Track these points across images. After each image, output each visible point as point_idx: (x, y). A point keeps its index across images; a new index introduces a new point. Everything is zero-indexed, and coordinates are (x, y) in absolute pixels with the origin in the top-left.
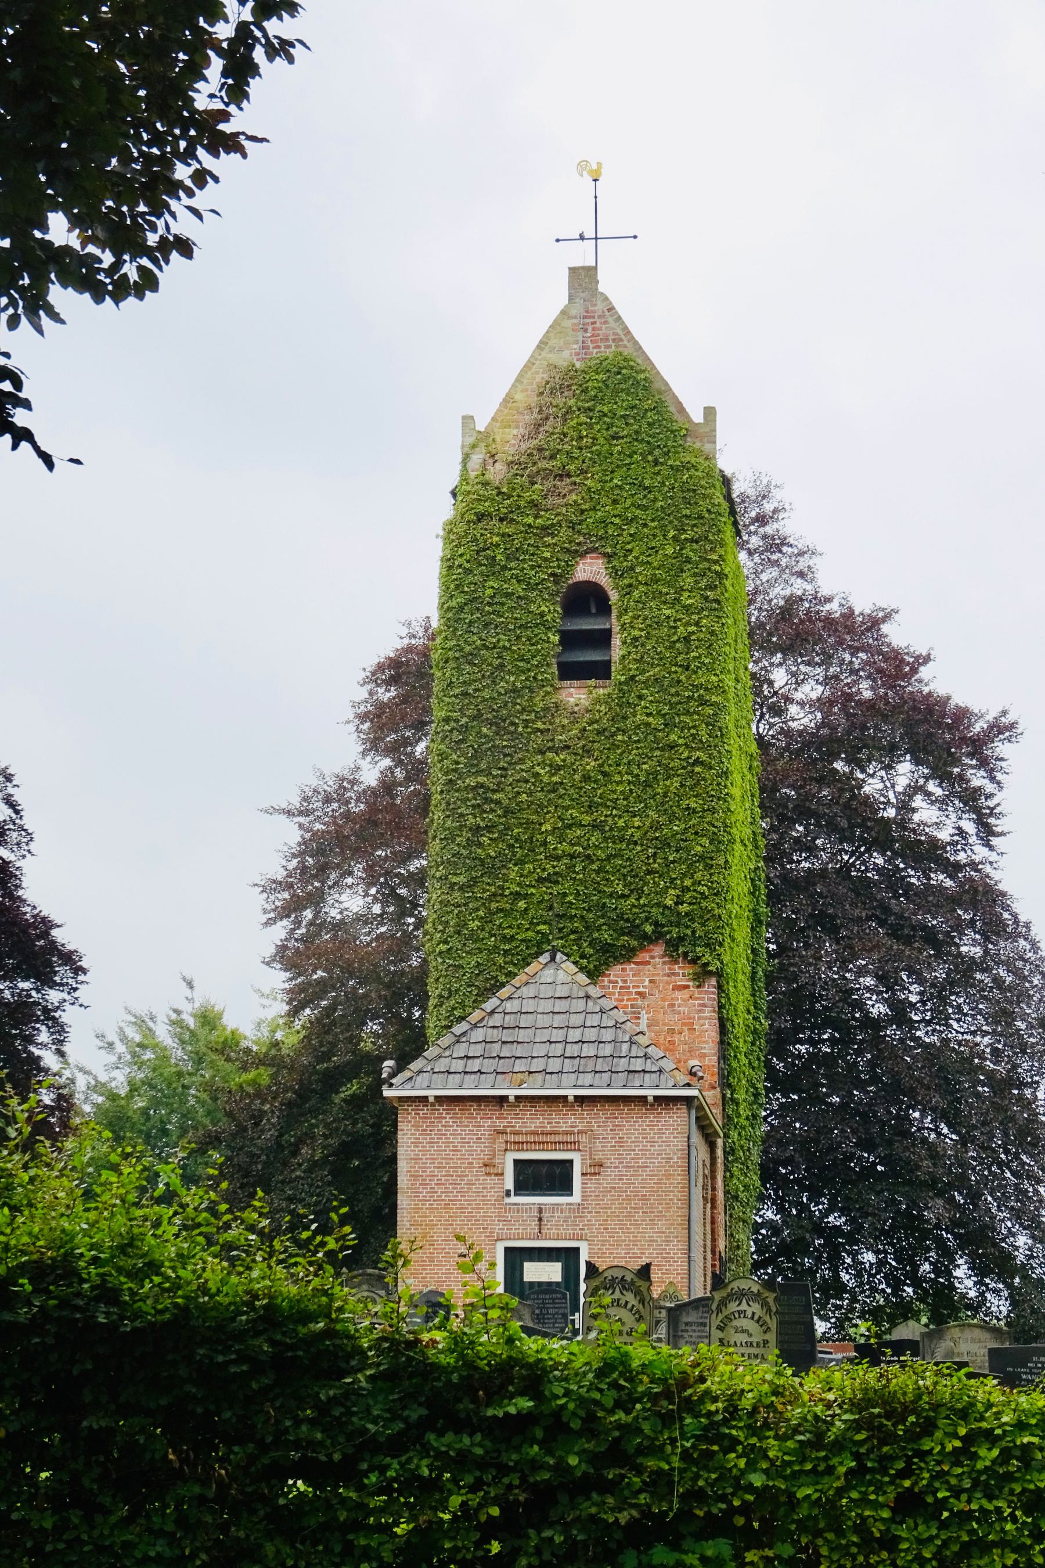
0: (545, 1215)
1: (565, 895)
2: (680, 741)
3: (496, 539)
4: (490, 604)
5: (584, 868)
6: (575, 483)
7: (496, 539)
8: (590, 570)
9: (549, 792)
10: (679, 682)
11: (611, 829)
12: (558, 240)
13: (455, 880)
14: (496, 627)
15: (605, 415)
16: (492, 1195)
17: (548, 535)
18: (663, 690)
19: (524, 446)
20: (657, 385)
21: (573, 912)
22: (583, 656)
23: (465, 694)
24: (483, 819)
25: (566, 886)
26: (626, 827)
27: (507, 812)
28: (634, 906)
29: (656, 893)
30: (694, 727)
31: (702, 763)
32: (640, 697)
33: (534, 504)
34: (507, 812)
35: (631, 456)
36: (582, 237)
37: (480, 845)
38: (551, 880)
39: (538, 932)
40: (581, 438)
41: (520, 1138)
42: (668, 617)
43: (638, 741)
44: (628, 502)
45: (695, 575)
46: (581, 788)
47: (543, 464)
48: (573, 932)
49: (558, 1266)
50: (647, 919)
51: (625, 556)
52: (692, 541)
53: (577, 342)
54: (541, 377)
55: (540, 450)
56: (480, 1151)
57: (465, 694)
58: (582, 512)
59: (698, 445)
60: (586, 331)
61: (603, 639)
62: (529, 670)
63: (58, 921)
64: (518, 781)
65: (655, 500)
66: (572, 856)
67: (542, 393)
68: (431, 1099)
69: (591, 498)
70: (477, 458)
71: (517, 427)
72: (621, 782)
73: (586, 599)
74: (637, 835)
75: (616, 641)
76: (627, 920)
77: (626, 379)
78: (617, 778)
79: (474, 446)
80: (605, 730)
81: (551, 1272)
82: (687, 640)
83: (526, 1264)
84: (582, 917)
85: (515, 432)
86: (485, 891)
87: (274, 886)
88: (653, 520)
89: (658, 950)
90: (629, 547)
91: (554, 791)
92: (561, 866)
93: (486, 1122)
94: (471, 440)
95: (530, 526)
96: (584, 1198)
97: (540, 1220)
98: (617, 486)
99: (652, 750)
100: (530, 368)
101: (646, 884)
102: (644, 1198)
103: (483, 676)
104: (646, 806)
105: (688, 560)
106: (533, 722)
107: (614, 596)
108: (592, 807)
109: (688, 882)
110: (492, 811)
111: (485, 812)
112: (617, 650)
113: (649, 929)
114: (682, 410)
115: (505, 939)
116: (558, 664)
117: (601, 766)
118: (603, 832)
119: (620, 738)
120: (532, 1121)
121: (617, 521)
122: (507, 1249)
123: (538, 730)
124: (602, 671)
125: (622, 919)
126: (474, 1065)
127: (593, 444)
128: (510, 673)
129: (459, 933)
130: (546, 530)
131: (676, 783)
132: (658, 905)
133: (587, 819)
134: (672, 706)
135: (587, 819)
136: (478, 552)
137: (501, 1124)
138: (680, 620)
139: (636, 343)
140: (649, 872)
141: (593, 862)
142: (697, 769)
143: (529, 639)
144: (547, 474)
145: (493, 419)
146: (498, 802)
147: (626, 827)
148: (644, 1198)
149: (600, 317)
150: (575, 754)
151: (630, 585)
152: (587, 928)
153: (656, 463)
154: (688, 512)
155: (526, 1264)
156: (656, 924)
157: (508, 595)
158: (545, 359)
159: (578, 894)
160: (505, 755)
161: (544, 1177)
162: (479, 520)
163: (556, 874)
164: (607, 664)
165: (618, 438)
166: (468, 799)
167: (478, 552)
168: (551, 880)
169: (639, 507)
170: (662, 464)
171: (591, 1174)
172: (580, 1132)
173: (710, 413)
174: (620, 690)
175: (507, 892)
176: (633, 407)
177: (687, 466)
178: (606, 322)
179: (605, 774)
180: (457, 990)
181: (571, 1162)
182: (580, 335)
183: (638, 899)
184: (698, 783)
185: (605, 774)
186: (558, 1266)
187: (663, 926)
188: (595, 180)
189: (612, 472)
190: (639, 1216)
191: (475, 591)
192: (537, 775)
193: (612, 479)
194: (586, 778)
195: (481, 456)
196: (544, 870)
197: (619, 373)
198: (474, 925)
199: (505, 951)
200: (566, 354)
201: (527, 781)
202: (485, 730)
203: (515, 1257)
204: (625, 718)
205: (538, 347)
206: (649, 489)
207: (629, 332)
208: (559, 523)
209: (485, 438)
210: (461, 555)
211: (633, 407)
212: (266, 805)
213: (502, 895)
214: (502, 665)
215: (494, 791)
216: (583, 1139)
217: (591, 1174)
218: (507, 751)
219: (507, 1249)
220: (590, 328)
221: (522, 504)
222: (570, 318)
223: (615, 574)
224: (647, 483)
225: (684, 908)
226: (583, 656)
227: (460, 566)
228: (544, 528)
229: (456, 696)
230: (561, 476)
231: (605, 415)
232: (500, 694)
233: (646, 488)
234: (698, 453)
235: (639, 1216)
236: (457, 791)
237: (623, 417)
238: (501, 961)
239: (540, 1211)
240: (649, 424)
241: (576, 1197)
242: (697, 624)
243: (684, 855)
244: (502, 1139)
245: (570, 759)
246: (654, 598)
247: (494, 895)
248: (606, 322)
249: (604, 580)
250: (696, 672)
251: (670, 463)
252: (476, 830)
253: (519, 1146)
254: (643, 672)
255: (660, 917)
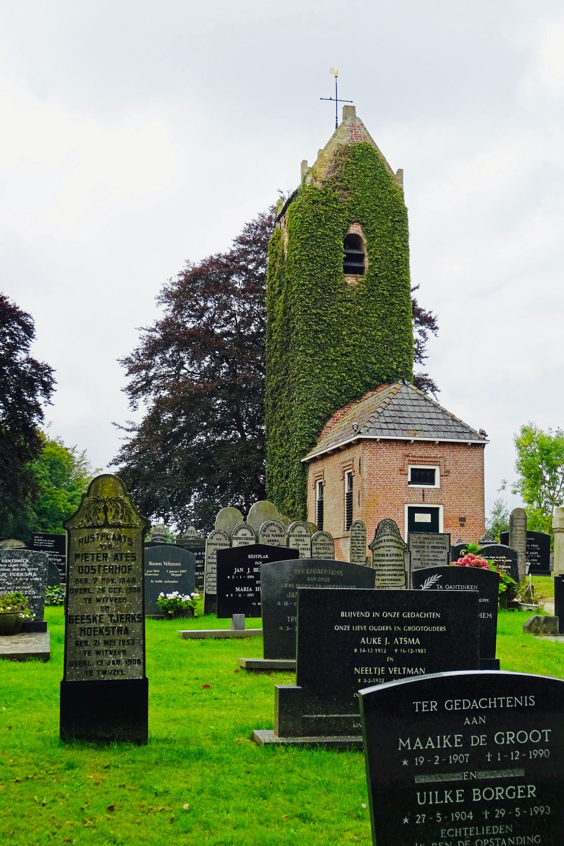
0: (426, 493)
1: (351, 361)
2: (396, 302)
3: (322, 212)
4: (319, 238)
5: (359, 351)
6: (350, 193)
7: (322, 212)
8: (355, 229)
9: (344, 318)
10: (394, 278)
11: (370, 336)
12: (321, 99)
13: (309, 352)
14: (322, 248)
15: (362, 167)
16: (403, 484)
17: (341, 213)
18: (388, 280)
19: (329, 176)
20: (380, 158)
21: (355, 369)
22: (353, 265)
23: (311, 275)
24: (319, 327)
25: (352, 358)
26: (375, 336)
27: (329, 325)
28: (378, 368)
29: (388, 363)
30: (402, 297)
31: (405, 312)
32: (380, 283)
33: (335, 199)
34: (329, 325)
35: (372, 185)
36: (331, 99)
37: (319, 338)
38: (346, 355)
39: (341, 376)
40: (353, 175)
42: (390, 251)
43: (379, 301)
44: (372, 203)
45: (400, 235)
46: (357, 318)
47: (338, 184)
48: (354, 377)
49: (417, 520)
50: (384, 373)
51: (371, 225)
52: (398, 221)
53: (349, 136)
54: (335, 148)
55: (337, 178)
56: (398, 464)
57: (311, 275)
58: (354, 205)
59: (397, 184)
60: (352, 132)
61: (360, 258)
62: (335, 267)
63: (53, 368)
64: (332, 313)
65: (383, 203)
66: (354, 346)
67: (336, 155)
68: (378, 440)
69: (358, 200)
70: (309, 178)
71: (325, 168)
72: (373, 317)
73: (353, 242)
75: (366, 259)
76: (376, 374)
77: (370, 153)
78: (371, 315)
79: (308, 173)
80: (365, 295)
81: (426, 518)
82: (397, 261)
83: (430, 515)
84: (358, 371)
85: (324, 169)
86: (320, 357)
87: (128, 361)
88: (382, 212)
90: (373, 221)
91: (346, 318)
92: (350, 349)
93: (400, 451)
94: (306, 171)
95: (334, 208)
96: (441, 485)
97: (423, 495)
98: (368, 196)
99: (385, 304)
100: (330, 144)
101: (383, 359)
102: (466, 487)
103: (317, 268)
104: (383, 328)
105: (397, 229)
106: (337, 289)
107: (365, 241)
108: (361, 326)
109: (401, 360)
110: (322, 324)
111: (320, 324)
112: (367, 263)
113: (385, 378)
114: (390, 169)
115: (329, 378)
116: (344, 266)
117: (365, 309)
118: (366, 336)
119: (372, 299)
120: (419, 452)
121: (368, 210)
122: (409, 508)
123: (339, 292)
124: (360, 271)
125: (374, 373)
126: (391, 426)
127: (358, 178)
128: (328, 268)
129: (310, 374)
130: (341, 211)
131: (395, 319)
132: (388, 368)
133: (360, 331)
134: (392, 287)
135: (360, 331)
136: (314, 216)
137: (407, 452)
138: (394, 253)
139: (372, 140)
140: (385, 354)
141: (362, 349)
142: (403, 314)
143: (335, 254)
144: (340, 188)
145: (315, 163)
146: (325, 321)
147: (375, 336)
148: (466, 487)
149: (358, 127)
150: (354, 304)
151: (373, 237)
152: (360, 376)
153: (383, 189)
154: (396, 210)
155: (430, 515)
156: (387, 376)
157: (327, 236)
158: (336, 141)
159: (357, 361)
160: (327, 302)
161: (423, 477)
162: (313, 204)
163: (348, 352)
164: (363, 268)
165: (368, 177)
166: (312, 318)
167: (314, 216)
168: (346, 355)
169: (376, 206)
170: (385, 189)
171: (445, 476)
172: (440, 457)
173: (400, 171)
174: (371, 279)
175: (330, 358)
176: (373, 165)
177: (395, 191)
178: (360, 130)
179: (366, 313)
180: (310, 398)
183: (380, 365)
184: (403, 320)
185: (366, 313)
186: (417, 520)
187: (390, 377)
188: (336, 77)
189: (366, 190)
190: (464, 495)
191: (313, 233)
192: (339, 311)
193: (366, 193)
194: (359, 314)
195: (311, 178)
196: (343, 350)
197: (367, 150)
198: (317, 371)
199: (329, 383)
200: (344, 140)
201: (336, 313)
202: (319, 290)
203: (413, 511)
205: (333, 136)
206: (380, 199)
207: (369, 135)
208: (345, 208)
209: (312, 170)
210: (307, 217)
211: (373, 165)
212: (139, 326)
213: (327, 360)
214: (324, 264)
215: (323, 316)
216: (442, 460)
217: (445, 476)
218: (328, 300)
219: (409, 508)
220: (354, 131)
221: (331, 199)
222: (346, 126)
223: (366, 232)
224: (380, 196)
225: (399, 370)
226: (353, 265)
227: (307, 221)
228: (340, 210)
229: (307, 275)
230: (344, 189)
231: (362, 167)
232: (324, 276)
233: (379, 198)
234: (397, 186)
235: (464, 495)
236: (308, 315)
237: (369, 168)
238: (327, 386)
239: (423, 491)
240: (380, 173)
241: (437, 485)
242: (401, 255)
243: (399, 348)
245: (353, 306)
246: (384, 243)
247: (324, 359)
248: (360, 130)
249: (361, 234)
250: (401, 275)
251: (388, 189)
252: (316, 332)
254: (380, 273)
255: (389, 373)
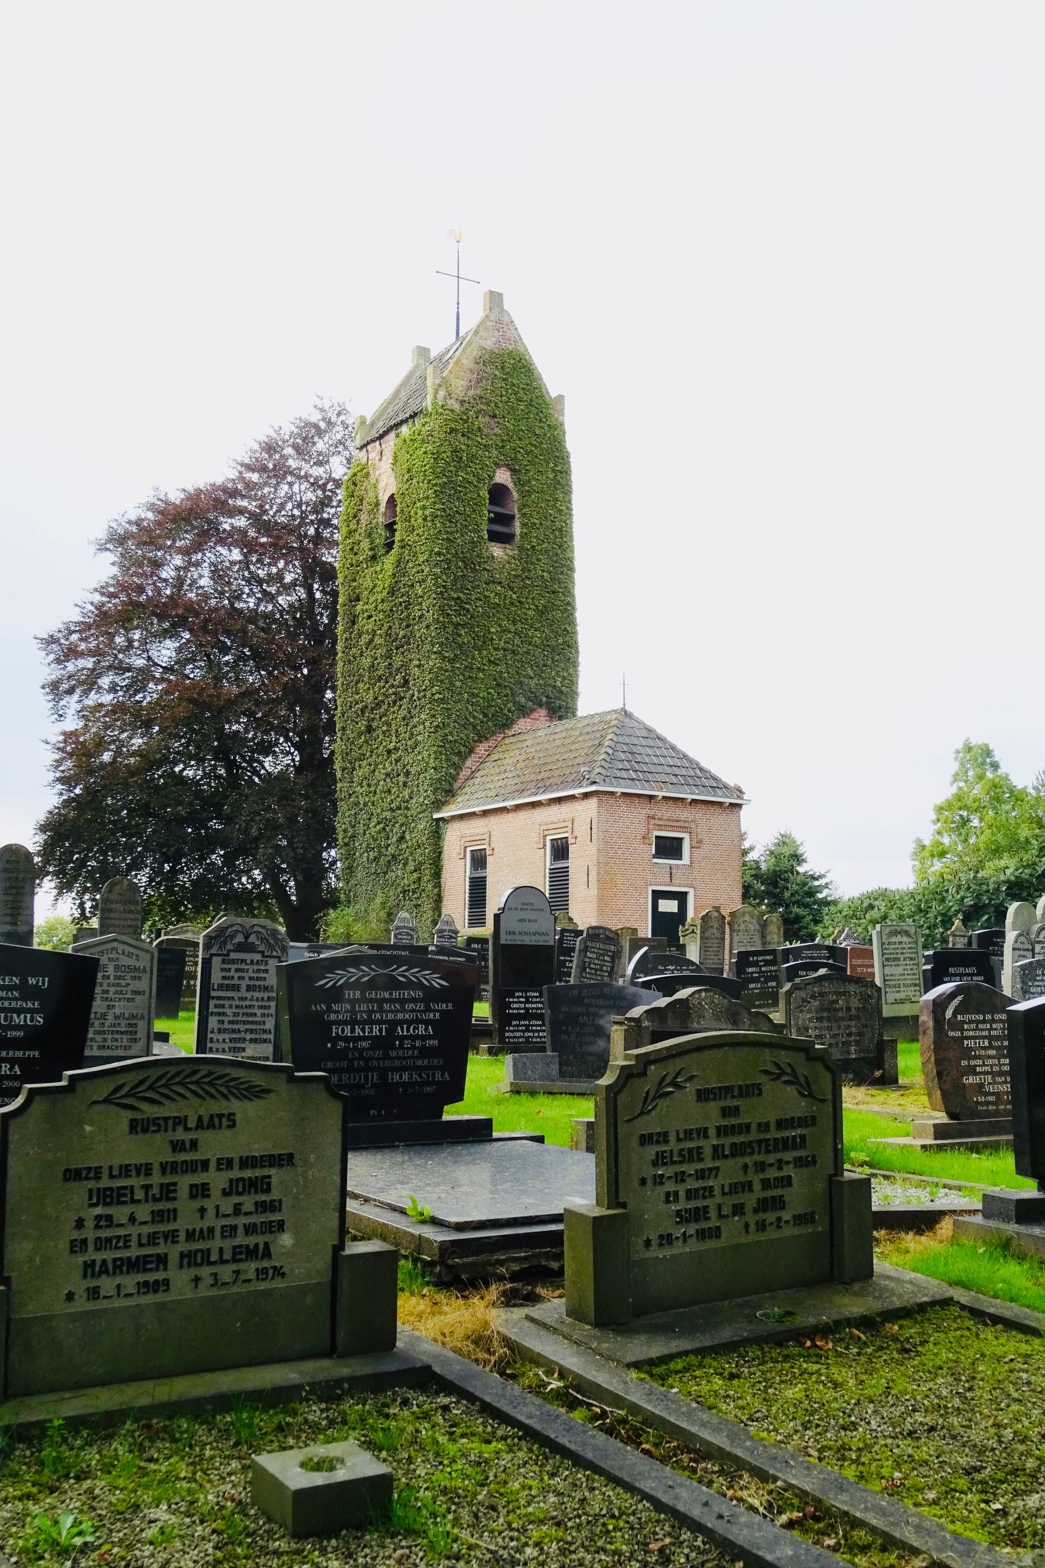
3: (463, 447)
8: (503, 476)
18: (549, 558)
23: (448, 539)
32: (538, 560)
39: (489, 693)
40: (501, 396)
41: (661, 823)
54: (476, 353)
55: (481, 398)
74: (539, 642)
79: (440, 386)
89: (543, 712)
114: (548, 393)
120: (667, 812)
140: (545, 665)
161: (669, 848)
169: (532, 445)
179: (520, 602)
181: (681, 840)
182: (496, 333)
185: (520, 602)
200: (489, 342)
203: (657, 895)
204: (529, 571)
244: (652, 822)
252: (457, 625)
253: (660, 827)
